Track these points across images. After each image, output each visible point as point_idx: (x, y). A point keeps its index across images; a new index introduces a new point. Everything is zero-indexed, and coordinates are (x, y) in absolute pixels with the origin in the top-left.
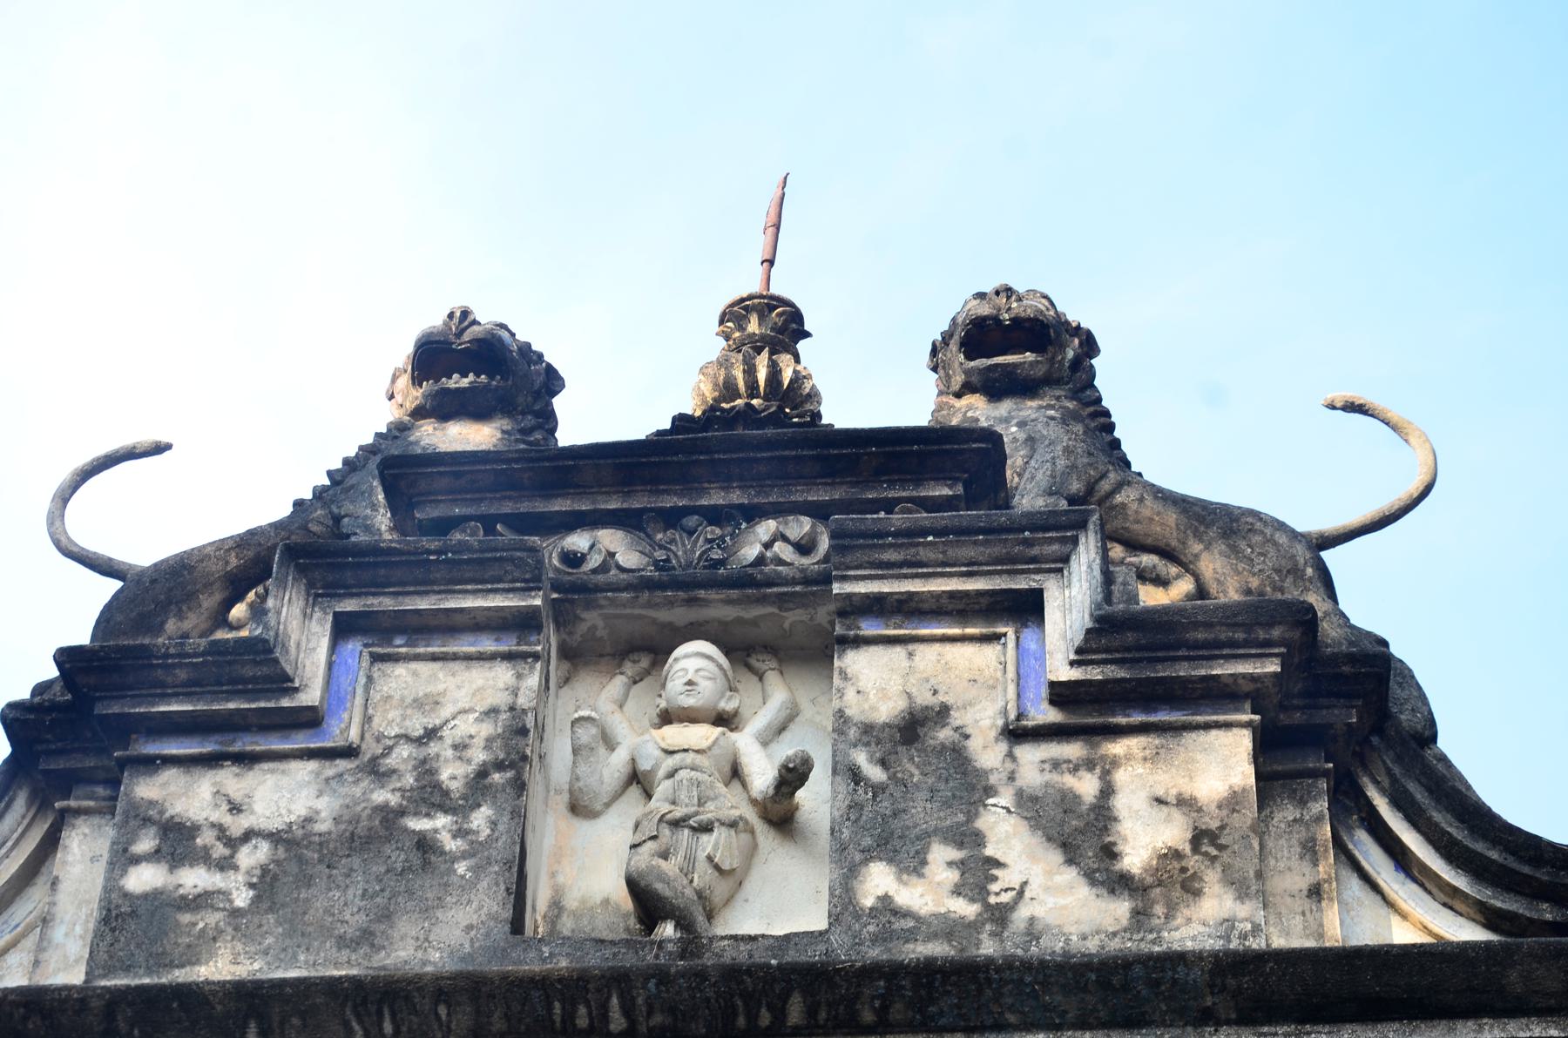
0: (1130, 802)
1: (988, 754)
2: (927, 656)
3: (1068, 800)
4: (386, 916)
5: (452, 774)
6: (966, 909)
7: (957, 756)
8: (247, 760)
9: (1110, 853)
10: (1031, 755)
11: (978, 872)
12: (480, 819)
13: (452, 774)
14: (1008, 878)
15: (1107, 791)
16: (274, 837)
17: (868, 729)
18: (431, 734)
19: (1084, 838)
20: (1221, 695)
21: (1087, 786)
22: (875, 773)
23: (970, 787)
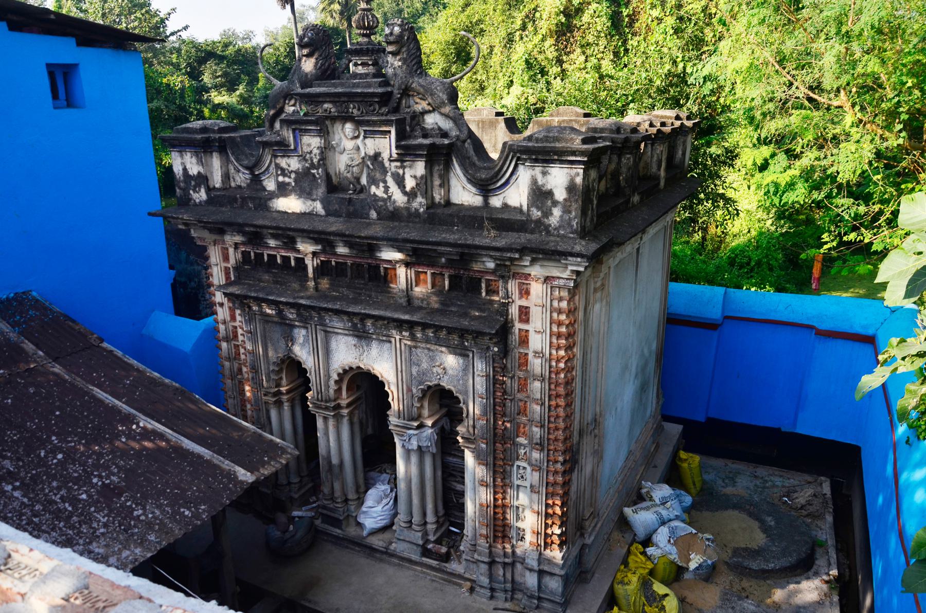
0: (407, 177)
1: (387, 164)
2: (377, 140)
3: (398, 174)
4: (311, 189)
5: (315, 161)
6: (385, 196)
7: (382, 163)
8: (289, 156)
9: (405, 187)
10: (394, 164)
11: (387, 188)
12: (320, 170)
13: (315, 161)
14: (391, 190)
15: (404, 173)
16: (295, 172)
17: (370, 156)
18: (311, 152)
19: (400, 181)
20: (421, 156)
21: (401, 172)
22: (371, 167)
23: (384, 171)
